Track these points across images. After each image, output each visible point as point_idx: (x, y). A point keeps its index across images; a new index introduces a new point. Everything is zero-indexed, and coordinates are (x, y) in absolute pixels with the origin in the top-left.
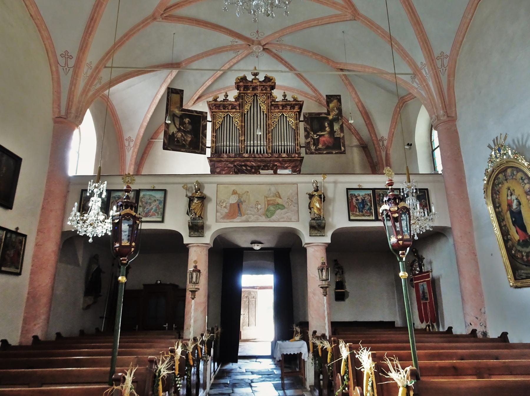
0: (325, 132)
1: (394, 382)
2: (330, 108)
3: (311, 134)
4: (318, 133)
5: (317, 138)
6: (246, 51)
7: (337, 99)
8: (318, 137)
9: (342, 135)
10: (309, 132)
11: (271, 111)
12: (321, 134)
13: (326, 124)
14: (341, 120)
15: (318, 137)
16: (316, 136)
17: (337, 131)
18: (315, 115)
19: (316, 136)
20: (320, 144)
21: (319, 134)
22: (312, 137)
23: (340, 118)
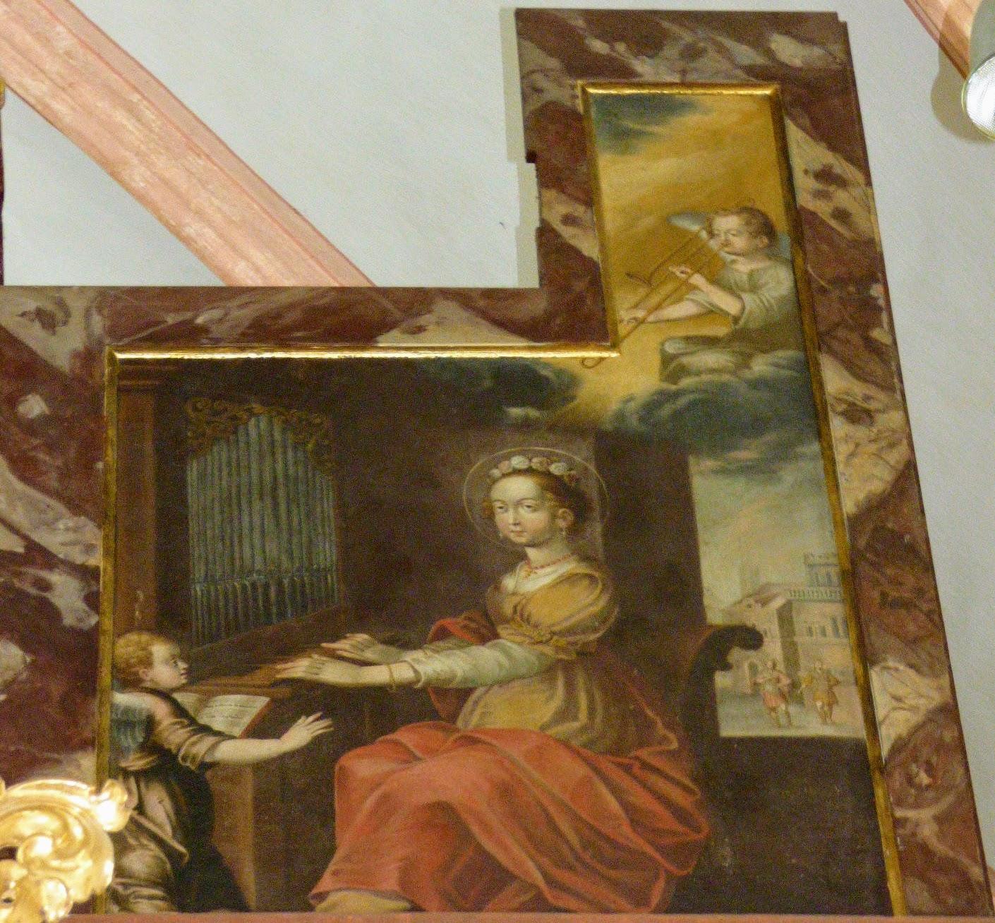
0: (486, 633)
1: (430, 636)
2: (611, 222)
3: (130, 682)
4: (300, 668)
5: (260, 767)
6: (209, 458)
7: (758, 75)
8: (301, 733)
9: (94, 620)
10: (87, 642)
11: (899, 813)
12: (377, 675)
13: (518, 488)
14: (858, 414)
15: (301, 733)
16: (262, 728)
17: (764, 620)
18: (260, 332)
19: (262, 728)
20: (362, 881)
21: (334, 674)
22: (152, 746)
23: (835, 380)
